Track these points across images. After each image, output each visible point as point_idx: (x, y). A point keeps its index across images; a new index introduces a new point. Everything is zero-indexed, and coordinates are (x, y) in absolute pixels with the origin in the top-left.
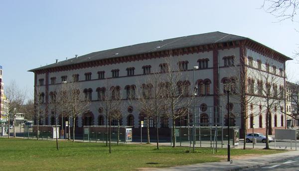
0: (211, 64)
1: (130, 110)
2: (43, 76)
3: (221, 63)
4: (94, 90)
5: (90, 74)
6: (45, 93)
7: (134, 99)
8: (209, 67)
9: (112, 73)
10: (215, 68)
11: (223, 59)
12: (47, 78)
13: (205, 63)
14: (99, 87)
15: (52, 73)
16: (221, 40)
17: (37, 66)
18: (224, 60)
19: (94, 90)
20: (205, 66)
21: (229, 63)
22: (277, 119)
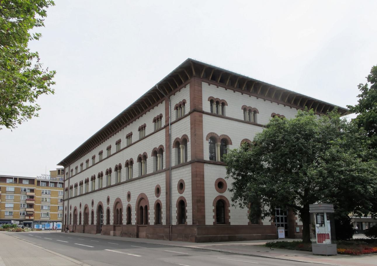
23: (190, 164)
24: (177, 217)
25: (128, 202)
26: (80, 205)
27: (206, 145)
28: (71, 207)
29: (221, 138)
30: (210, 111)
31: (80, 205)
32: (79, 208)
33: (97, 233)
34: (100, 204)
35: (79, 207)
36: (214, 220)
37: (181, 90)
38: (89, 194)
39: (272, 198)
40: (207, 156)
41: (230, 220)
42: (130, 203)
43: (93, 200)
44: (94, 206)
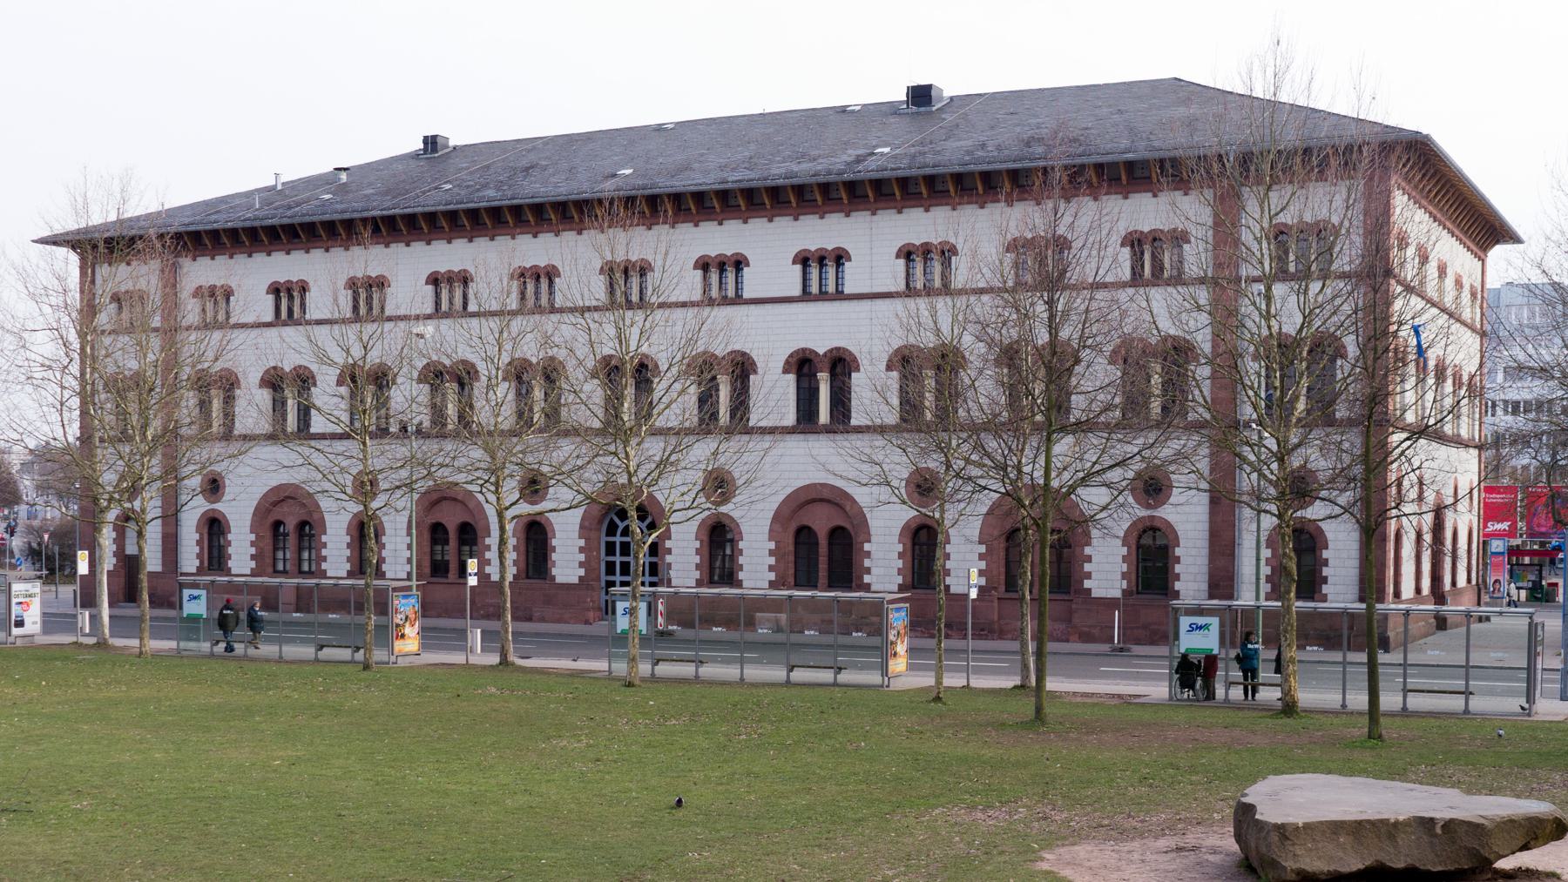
0: (1196, 258)
1: (720, 484)
2: (142, 276)
3: (191, 311)
4: (251, 376)
5: (380, 283)
6: (1203, 341)
7: (227, 435)
8: (746, 295)
9: (271, 297)
10: (171, 331)
11: (695, 267)
12: (1225, 232)
13: (937, 268)
14: (810, 345)
15: (204, 262)
16: (1290, 138)
17: (100, 214)
18: (699, 273)
19: (251, 376)
20: (831, 288)
21: (1158, 268)
22: (1466, 577)
41: (230, 563)
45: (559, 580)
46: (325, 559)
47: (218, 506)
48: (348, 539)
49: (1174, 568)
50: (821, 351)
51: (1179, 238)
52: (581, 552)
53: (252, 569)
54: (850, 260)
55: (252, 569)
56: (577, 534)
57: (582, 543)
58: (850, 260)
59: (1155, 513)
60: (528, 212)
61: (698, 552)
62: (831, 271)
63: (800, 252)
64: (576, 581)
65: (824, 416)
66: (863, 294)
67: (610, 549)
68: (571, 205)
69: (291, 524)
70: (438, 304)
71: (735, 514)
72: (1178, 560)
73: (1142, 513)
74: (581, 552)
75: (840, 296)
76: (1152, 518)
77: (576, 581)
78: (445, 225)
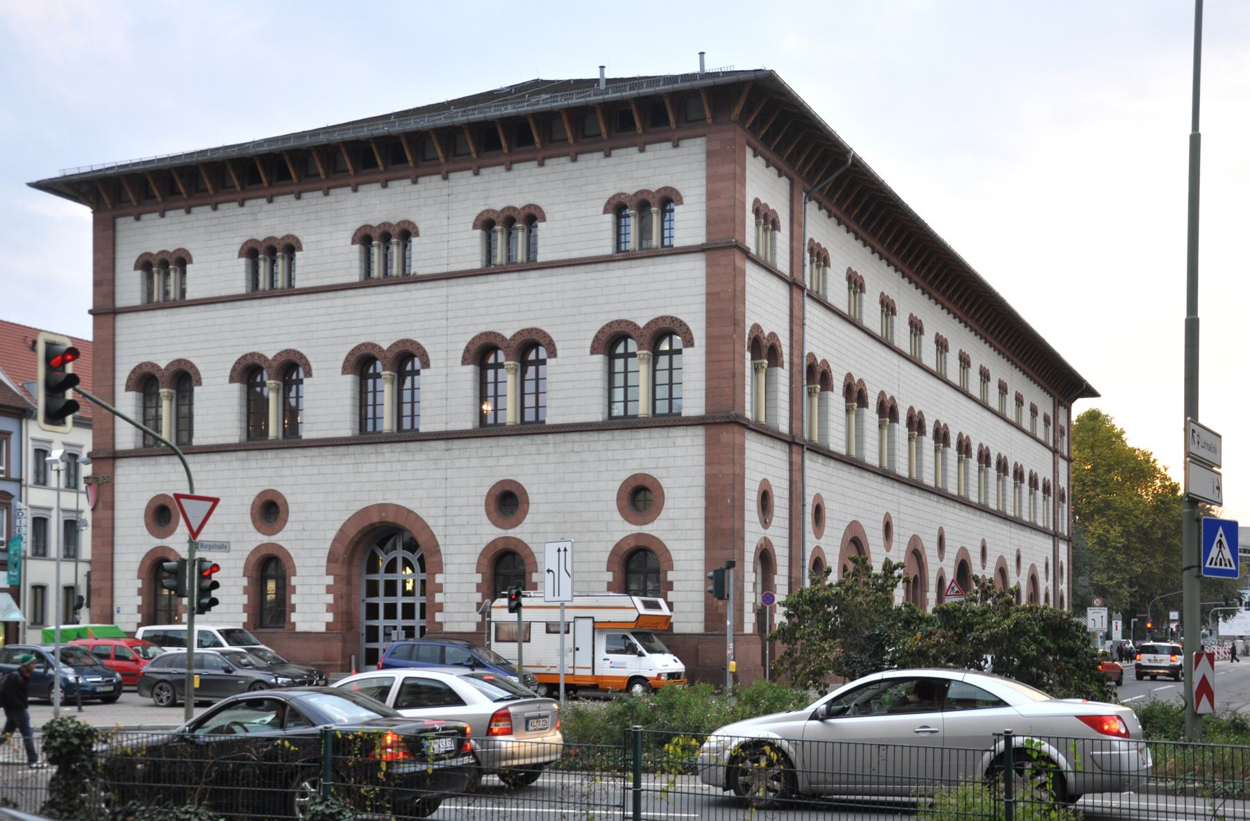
3: (130, 287)
8: (299, 284)
13: (521, 237)
20: (395, 270)
23: (701, 427)
24: (754, 624)
25: (822, 546)
26: (941, 540)
27: (127, 402)
28: (818, 511)
29: (283, 243)
30: (1060, 463)
31: (941, 540)
32: (1015, 574)
33: (815, 711)
34: (965, 558)
35: (881, 534)
36: (244, 618)
37: (547, 162)
38: (890, 483)
39: (889, 600)
40: (126, 437)
41: (294, 617)
42: (822, 543)
43: (941, 529)
44: (946, 555)
45: (300, 628)
46: (440, 608)
47: (277, 539)
48: (478, 578)
49: (290, 598)
50: (163, 364)
51: (668, 200)
52: (328, 592)
53: (328, 624)
54: (682, 203)
55: (328, 624)
56: (324, 570)
57: (330, 580)
58: (682, 203)
59: (646, 529)
60: (128, 190)
61: (246, 590)
62: (281, 265)
63: (481, 214)
64: (322, 628)
65: (274, 430)
66: (438, 275)
67: (372, 589)
68: (229, 166)
69: (562, 549)
70: (150, 293)
71: (526, 539)
72: (329, 589)
73: (499, 533)
74: (328, 592)
75: (407, 278)
76: (163, 548)
77: (322, 628)
78: (132, 197)
